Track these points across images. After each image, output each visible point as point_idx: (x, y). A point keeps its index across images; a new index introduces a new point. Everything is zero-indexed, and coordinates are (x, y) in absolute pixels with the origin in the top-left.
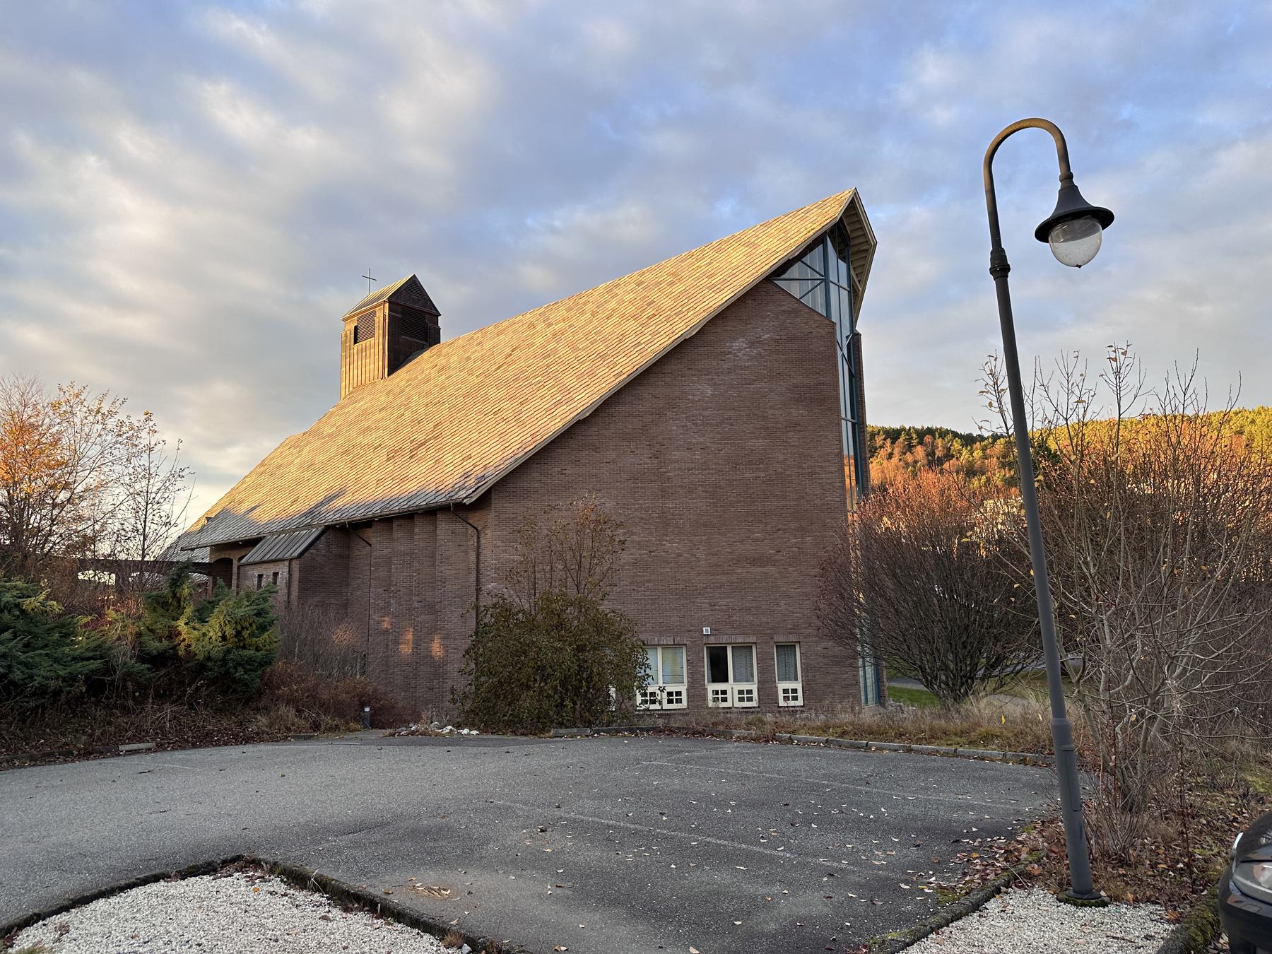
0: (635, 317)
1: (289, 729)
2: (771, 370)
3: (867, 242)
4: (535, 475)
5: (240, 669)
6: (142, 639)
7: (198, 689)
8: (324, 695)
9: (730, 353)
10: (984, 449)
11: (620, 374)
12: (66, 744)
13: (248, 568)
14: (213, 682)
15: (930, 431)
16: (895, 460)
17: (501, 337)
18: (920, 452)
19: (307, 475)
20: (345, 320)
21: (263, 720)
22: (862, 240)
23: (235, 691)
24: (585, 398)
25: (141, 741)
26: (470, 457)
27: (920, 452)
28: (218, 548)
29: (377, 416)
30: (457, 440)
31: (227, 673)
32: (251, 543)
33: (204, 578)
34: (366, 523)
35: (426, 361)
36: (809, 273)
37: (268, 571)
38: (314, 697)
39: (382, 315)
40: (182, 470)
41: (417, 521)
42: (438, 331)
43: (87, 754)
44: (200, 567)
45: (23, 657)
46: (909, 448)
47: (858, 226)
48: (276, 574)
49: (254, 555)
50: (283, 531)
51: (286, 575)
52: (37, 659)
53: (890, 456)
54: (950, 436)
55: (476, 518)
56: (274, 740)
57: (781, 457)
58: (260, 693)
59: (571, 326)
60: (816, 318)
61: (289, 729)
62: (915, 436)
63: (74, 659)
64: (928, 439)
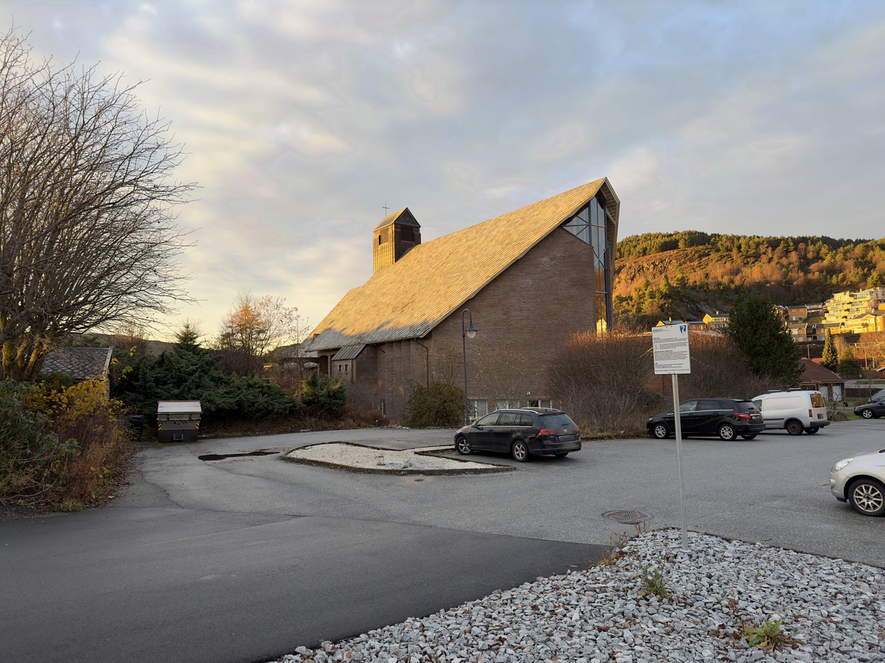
0: (501, 243)
4: (451, 324)
8: (362, 415)
10: (845, 253)
15: (804, 240)
16: (773, 263)
18: (794, 256)
19: (358, 317)
21: (343, 423)
27: (794, 256)
28: (321, 351)
29: (389, 287)
30: (420, 304)
32: (337, 349)
34: (383, 343)
35: (413, 254)
37: (343, 364)
39: (391, 230)
41: (403, 343)
43: (292, 432)
46: (787, 252)
53: (770, 260)
54: (820, 243)
55: (426, 343)
62: (791, 244)
64: (802, 246)
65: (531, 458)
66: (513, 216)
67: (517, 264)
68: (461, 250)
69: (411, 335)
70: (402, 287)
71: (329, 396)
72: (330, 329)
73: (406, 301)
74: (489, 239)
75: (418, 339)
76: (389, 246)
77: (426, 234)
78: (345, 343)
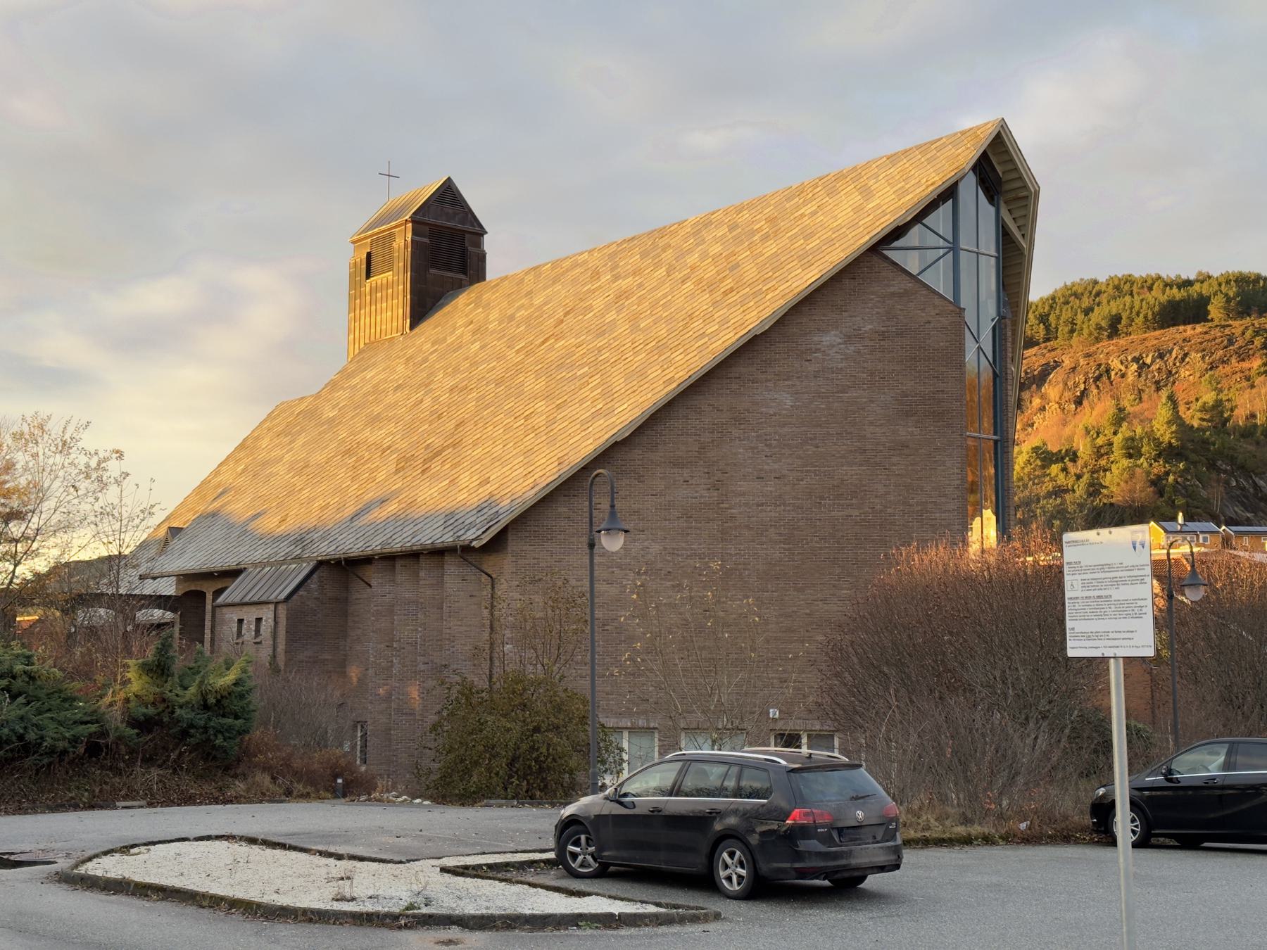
1: (263, 794)
2: (872, 374)
3: (1025, 187)
4: (561, 510)
5: (220, 736)
6: (130, 705)
7: (181, 754)
8: (297, 764)
9: (817, 350)
11: (671, 380)
12: (72, 798)
13: (225, 610)
14: (195, 748)
17: (558, 287)
20: (354, 242)
21: (240, 786)
22: (1018, 184)
23: (215, 758)
24: (627, 411)
25: (133, 799)
26: (487, 481)
29: (390, 399)
30: (478, 452)
31: (208, 740)
33: (169, 615)
34: (366, 560)
35: (462, 311)
36: (932, 240)
37: (250, 615)
38: (288, 766)
39: (403, 240)
40: (152, 506)
42: (482, 258)
44: (160, 601)
45: (35, 720)
47: (1010, 167)
48: (259, 620)
49: (234, 592)
50: (268, 563)
51: (271, 622)
52: (46, 722)
55: (490, 563)
56: (250, 801)
57: (881, 489)
58: (239, 760)
59: (640, 285)
60: (937, 301)
61: (263, 794)
63: (75, 722)
65: (762, 889)
66: (746, 215)
67: (750, 348)
68: (598, 303)
69: (448, 539)
70: (427, 402)
71: (206, 707)
72: (214, 515)
73: (436, 441)
74: (678, 275)
75: (467, 549)
76: (395, 282)
77: (501, 253)
78: (259, 555)
